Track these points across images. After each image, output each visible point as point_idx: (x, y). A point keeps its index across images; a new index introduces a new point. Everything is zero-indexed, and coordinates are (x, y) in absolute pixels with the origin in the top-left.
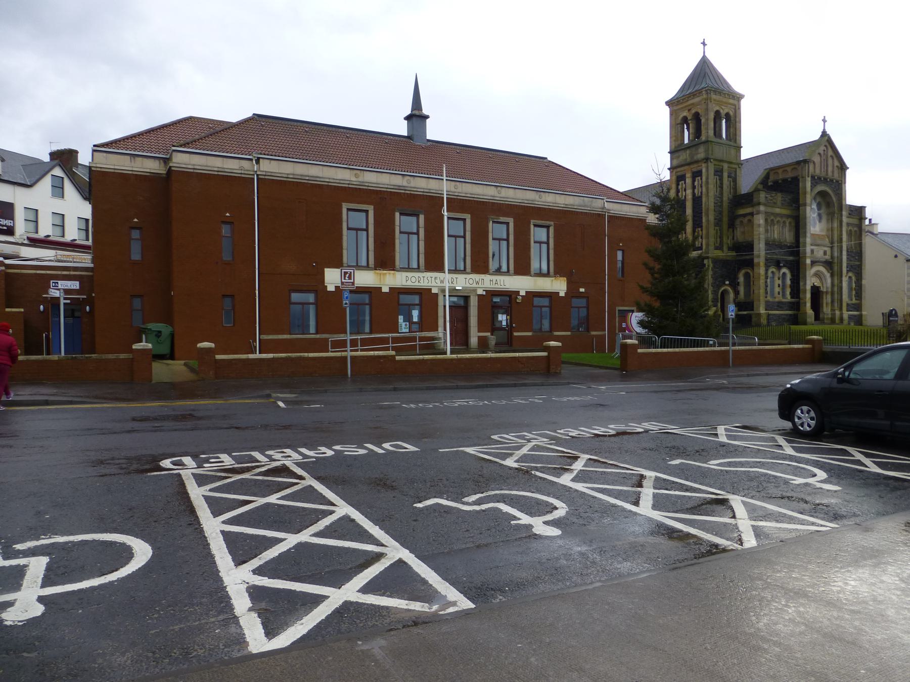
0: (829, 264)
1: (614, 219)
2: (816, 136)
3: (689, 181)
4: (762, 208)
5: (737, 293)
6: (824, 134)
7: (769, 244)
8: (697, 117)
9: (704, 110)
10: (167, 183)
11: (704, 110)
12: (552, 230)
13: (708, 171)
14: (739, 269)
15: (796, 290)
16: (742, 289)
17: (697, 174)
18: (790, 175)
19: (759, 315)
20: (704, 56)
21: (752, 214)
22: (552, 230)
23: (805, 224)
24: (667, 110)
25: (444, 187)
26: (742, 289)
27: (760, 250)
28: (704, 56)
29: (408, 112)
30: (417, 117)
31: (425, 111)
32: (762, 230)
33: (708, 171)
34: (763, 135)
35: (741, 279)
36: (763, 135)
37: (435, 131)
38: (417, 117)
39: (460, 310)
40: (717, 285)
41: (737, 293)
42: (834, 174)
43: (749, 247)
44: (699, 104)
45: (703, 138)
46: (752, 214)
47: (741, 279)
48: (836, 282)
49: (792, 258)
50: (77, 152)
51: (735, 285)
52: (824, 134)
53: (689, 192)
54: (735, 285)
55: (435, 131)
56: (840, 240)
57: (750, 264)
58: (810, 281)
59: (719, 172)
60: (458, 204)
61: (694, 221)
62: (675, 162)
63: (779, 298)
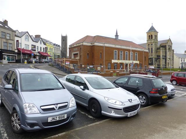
0: (170, 59)
1: (145, 52)
2: (168, 39)
3: (150, 45)
4: (162, 50)
5: (157, 63)
6: (170, 39)
7: (163, 56)
8: (152, 36)
9: (152, 34)
10: (92, 47)
11: (152, 34)
12: (137, 54)
13: (154, 44)
14: (158, 59)
15: (166, 63)
16: (158, 62)
17: (152, 44)
18: (165, 45)
19: (161, 67)
20: (152, 26)
21: (160, 51)
22: (137, 54)
23: (176, 68)
24: (146, 34)
25: (131, 48)
26: (158, 62)
27: (161, 56)
28: (152, 26)
29: (115, 35)
30: (117, 36)
31: (118, 35)
32: (162, 53)
33: (154, 44)
34: (162, 37)
35: (158, 61)
36: (162, 37)
37: (120, 38)
38: (117, 36)
39: (130, 65)
40: (155, 62)
41: (157, 63)
42: (171, 45)
43: (160, 56)
44: (152, 33)
45: (153, 39)
46: (160, 51)
47: (158, 61)
48: (113, 114)
49: (165, 58)
50: (40, 35)
51: (157, 62)
52: (170, 39)
53: (150, 47)
54: (157, 62)
55: (120, 38)
56: (171, 55)
57: (160, 59)
58: (167, 62)
59: (155, 44)
60: (132, 51)
61: (151, 52)
62: (148, 42)
63: (163, 64)
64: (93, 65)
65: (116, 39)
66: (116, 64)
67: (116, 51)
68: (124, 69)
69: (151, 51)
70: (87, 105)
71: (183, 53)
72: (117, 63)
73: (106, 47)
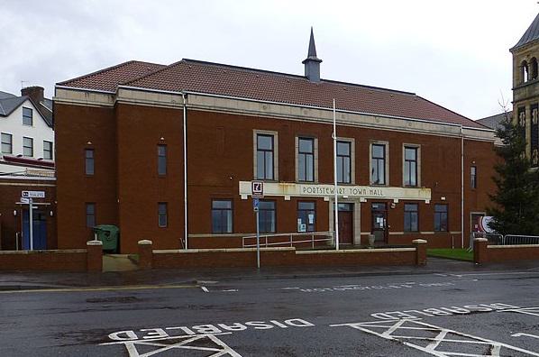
3: (528, 112)
10: (115, 113)
12: (419, 150)
22: (419, 150)
25: (334, 117)
30: (312, 61)
31: (319, 57)
37: (326, 73)
38: (312, 61)
53: (528, 120)
55: (326, 73)
60: (345, 130)
62: (517, 98)
64: (115, 222)
65: (310, 84)
66: (414, 208)
67: (271, 133)
68: (256, 252)
69: (258, 97)
70: (538, 355)
71: (481, 91)
72: (386, 203)
73: (194, 114)
